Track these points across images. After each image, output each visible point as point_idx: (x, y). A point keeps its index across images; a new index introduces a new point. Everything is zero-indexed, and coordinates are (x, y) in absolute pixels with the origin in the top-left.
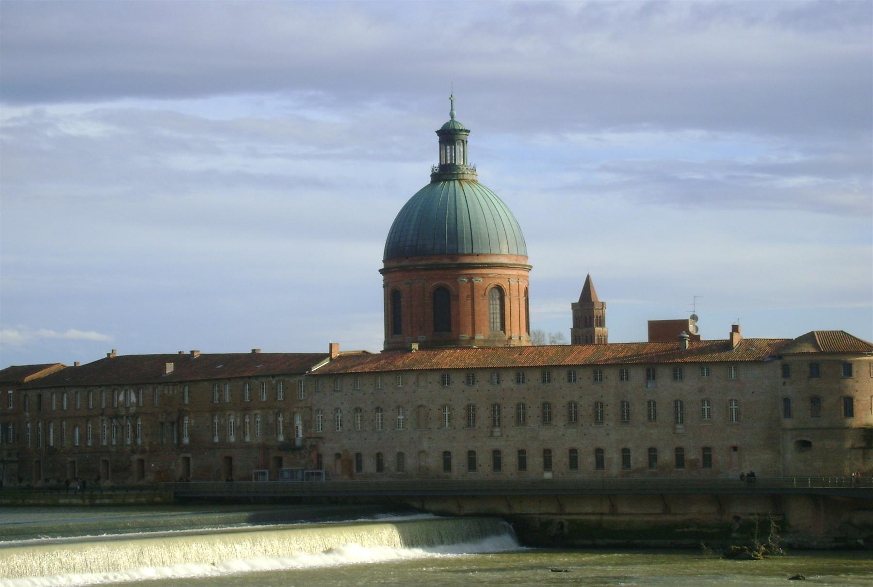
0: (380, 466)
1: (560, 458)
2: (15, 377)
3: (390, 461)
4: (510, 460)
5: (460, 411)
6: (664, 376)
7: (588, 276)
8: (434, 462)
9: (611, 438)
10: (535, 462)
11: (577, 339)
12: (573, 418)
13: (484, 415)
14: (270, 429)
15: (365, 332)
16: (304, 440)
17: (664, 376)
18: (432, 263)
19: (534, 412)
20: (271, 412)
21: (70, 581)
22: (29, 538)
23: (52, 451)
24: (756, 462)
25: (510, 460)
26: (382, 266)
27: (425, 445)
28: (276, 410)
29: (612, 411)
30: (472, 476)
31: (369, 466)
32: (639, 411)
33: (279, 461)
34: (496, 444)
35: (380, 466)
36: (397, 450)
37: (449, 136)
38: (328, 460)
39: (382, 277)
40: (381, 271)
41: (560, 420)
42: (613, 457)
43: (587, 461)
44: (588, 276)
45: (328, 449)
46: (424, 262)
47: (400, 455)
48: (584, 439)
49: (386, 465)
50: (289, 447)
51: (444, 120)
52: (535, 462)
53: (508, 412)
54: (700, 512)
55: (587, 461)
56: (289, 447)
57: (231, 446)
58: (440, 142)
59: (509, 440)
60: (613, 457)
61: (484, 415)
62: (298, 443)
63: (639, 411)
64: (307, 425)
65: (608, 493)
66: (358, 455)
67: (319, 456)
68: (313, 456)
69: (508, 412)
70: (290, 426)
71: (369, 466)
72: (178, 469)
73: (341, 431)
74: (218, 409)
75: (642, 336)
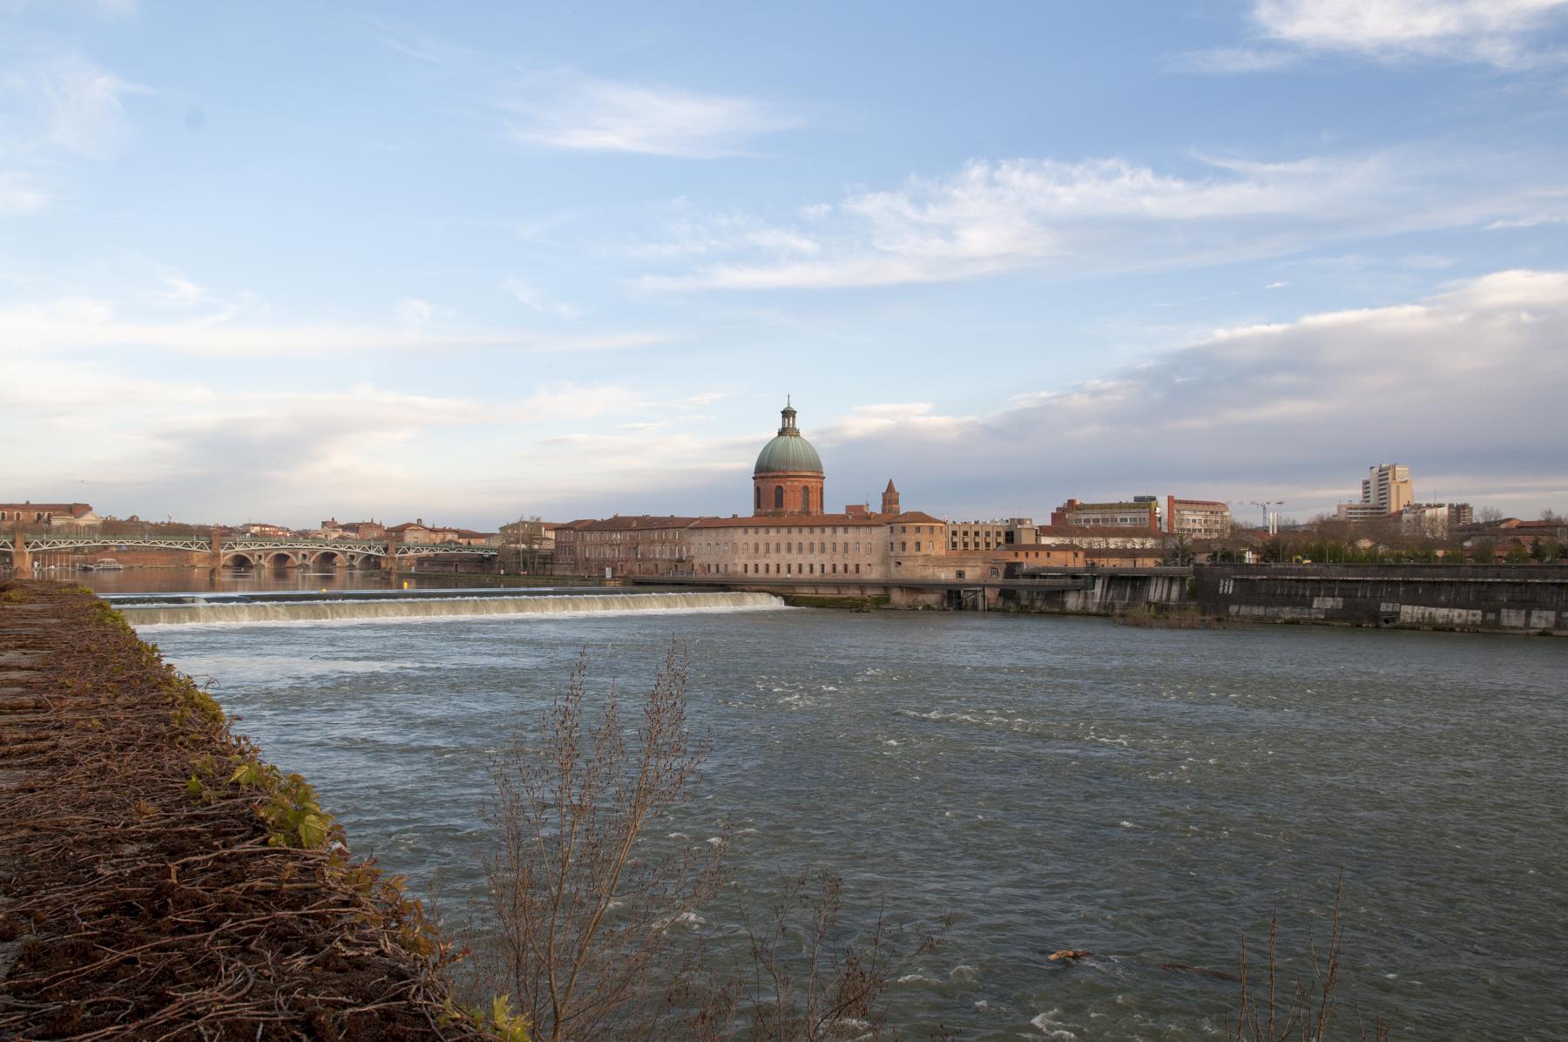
1: (794, 568)
3: (722, 568)
4: (773, 569)
5: (752, 546)
7: (890, 484)
8: (740, 569)
9: (817, 559)
10: (784, 569)
11: (884, 510)
12: (800, 550)
13: (762, 548)
14: (672, 552)
17: (840, 530)
19: (783, 547)
21: (960, 574)
23: (587, 560)
24: (875, 574)
29: (817, 547)
31: (713, 569)
32: (829, 547)
34: (789, 557)
37: (788, 414)
42: (817, 568)
43: (806, 569)
44: (890, 484)
45: (696, 562)
48: (805, 559)
50: (680, 560)
51: (783, 407)
52: (784, 569)
53: (772, 547)
54: (854, 593)
59: (773, 560)
60: (817, 568)
61: (762, 548)
63: (829, 547)
69: (772, 547)
71: (713, 569)
72: (636, 569)
73: (703, 552)
74: (652, 542)
75: (1132, 501)
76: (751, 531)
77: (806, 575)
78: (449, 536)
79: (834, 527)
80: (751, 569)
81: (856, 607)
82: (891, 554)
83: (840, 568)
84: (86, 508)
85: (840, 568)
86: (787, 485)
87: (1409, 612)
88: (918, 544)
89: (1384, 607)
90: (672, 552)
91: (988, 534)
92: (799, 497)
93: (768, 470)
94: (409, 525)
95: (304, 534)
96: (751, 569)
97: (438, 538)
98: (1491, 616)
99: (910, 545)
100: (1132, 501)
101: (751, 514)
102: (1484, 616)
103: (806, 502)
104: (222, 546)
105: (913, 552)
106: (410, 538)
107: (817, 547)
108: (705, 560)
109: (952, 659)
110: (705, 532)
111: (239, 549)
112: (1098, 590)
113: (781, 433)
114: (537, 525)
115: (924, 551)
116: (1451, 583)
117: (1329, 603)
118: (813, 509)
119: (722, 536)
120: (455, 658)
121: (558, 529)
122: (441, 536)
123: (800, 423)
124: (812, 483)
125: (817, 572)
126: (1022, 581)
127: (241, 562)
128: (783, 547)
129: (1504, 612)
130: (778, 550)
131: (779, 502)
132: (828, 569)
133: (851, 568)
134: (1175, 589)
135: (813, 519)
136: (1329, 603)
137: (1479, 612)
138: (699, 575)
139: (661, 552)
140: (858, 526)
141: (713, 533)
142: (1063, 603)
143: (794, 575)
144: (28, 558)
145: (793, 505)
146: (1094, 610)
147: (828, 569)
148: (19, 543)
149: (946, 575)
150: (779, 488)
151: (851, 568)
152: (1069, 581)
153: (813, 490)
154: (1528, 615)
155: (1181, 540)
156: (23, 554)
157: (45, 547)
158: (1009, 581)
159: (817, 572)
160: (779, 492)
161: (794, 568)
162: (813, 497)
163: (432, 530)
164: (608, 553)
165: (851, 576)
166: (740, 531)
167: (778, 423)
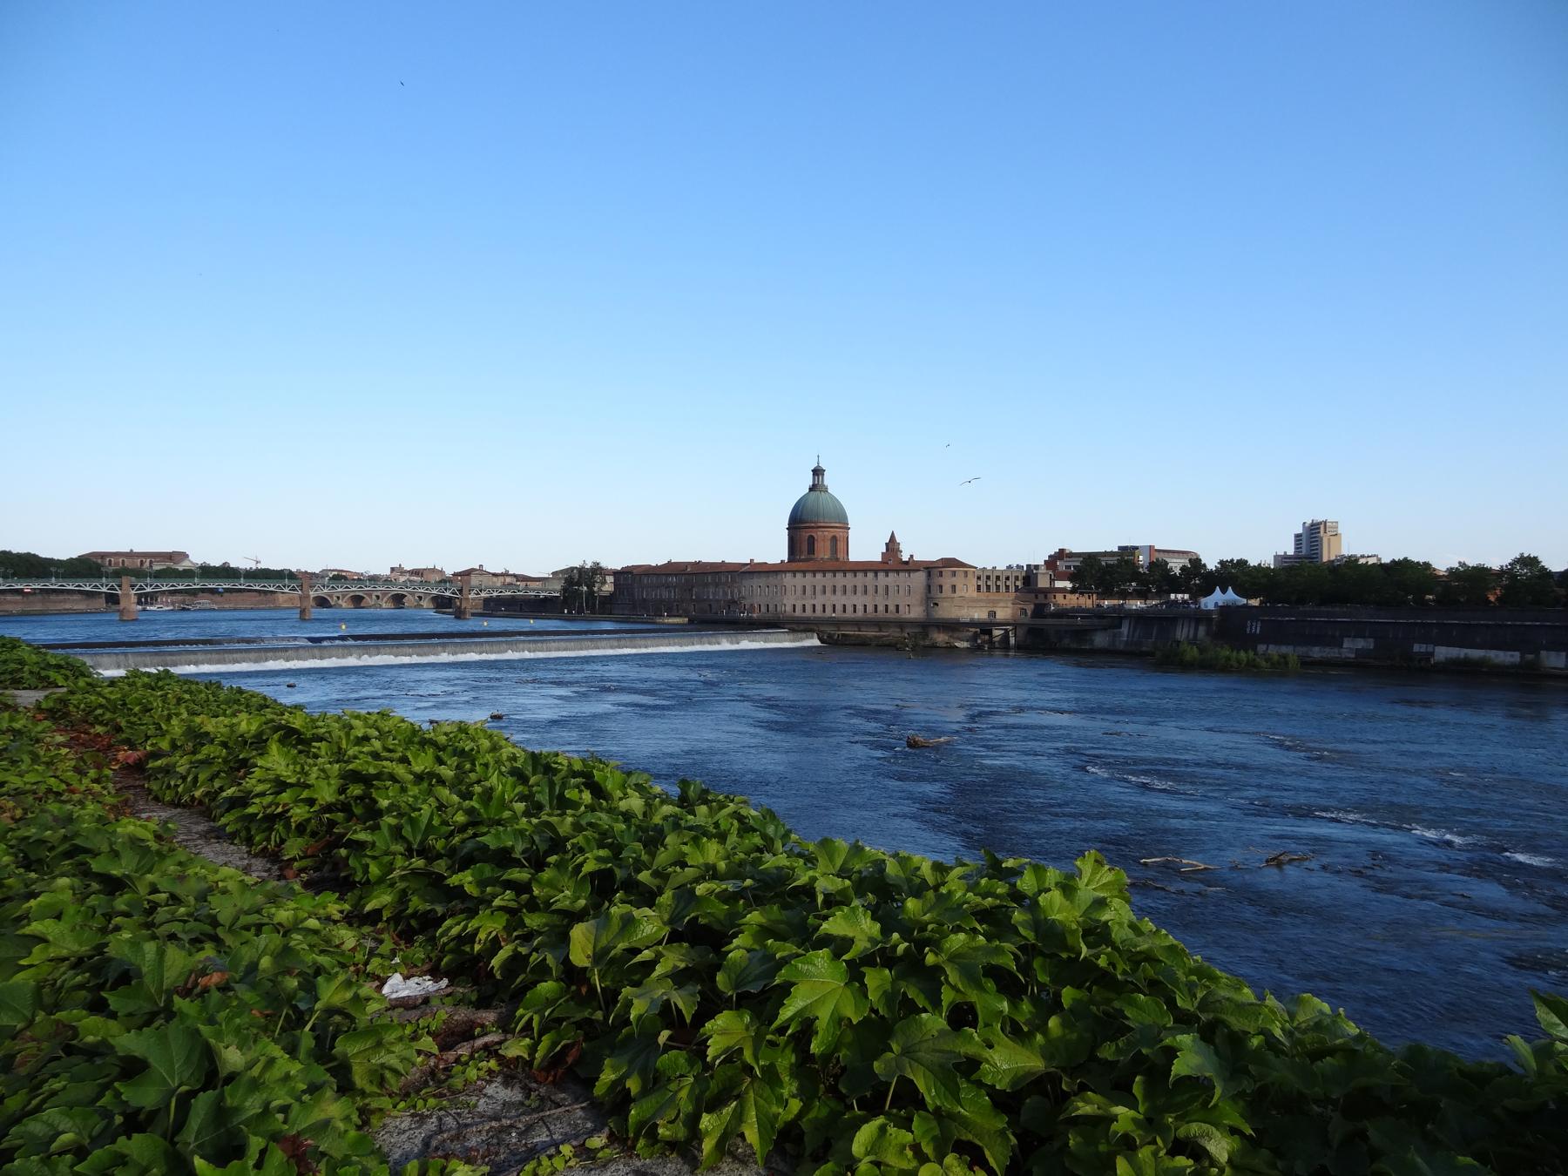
1: (839, 608)
2: (4, 553)
4: (819, 608)
5: (799, 589)
6: (881, 575)
7: (893, 536)
8: (789, 609)
9: (859, 600)
10: (829, 609)
15: (776, 550)
17: (881, 575)
18: (813, 528)
22: (305, 659)
25: (819, 608)
29: (860, 589)
30: (888, 615)
32: (871, 590)
34: (833, 598)
37: (818, 472)
41: (839, 593)
42: (860, 608)
43: (850, 609)
44: (893, 536)
51: (814, 465)
52: (829, 609)
53: (849, 588)
55: (850, 609)
59: (819, 601)
60: (860, 608)
63: (871, 590)
65: (857, 623)
73: (757, 596)
74: (707, 585)
77: (849, 614)
78: (508, 580)
79: (876, 572)
80: (799, 609)
81: (892, 646)
82: (930, 597)
83: (881, 608)
84: (184, 556)
85: (881, 608)
86: (818, 534)
87: (1442, 653)
88: (954, 587)
89: (1416, 648)
90: (725, 594)
91: (998, 578)
92: (828, 544)
93: (802, 521)
94: (473, 570)
95: (374, 579)
96: (799, 609)
97: (499, 582)
98: (1530, 657)
99: (947, 588)
103: (835, 550)
104: (312, 587)
105: (950, 594)
106: (474, 581)
107: (860, 589)
109: (414, 714)
111: (319, 593)
112: (1125, 630)
113: (813, 488)
114: (597, 570)
115: (958, 593)
116: (1487, 626)
117: (1361, 644)
118: (840, 556)
119: (772, 580)
120: (633, 672)
121: (616, 573)
122: (501, 579)
123: (828, 480)
124: (839, 533)
125: (860, 613)
126: (1050, 621)
127: (322, 602)
128: (828, 590)
129: (1543, 653)
130: (834, 592)
131: (811, 550)
132: (870, 609)
133: (892, 608)
134: (1202, 630)
136: (1361, 644)
137: (1517, 654)
140: (898, 571)
142: (1092, 641)
143: (839, 614)
144: (134, 599)
145: (823, 552)
146: (1122, 647)
147: (870, 609)
148: (125, 586)
149: (980, 614)
150: (834, 539)
151: (892, 608)
152: (1096, 621)
153: (839, 543)
155: (930, 597)
156: (128, 595)
157: (149, 590)
158: (1039, 621)
159: (819, 612)
160: (812, 540)
161: (839, 608)
162: (840, 545)
163: (495, 575)
164: (665, 595)
165: (891, 615)
166: (789, 575)
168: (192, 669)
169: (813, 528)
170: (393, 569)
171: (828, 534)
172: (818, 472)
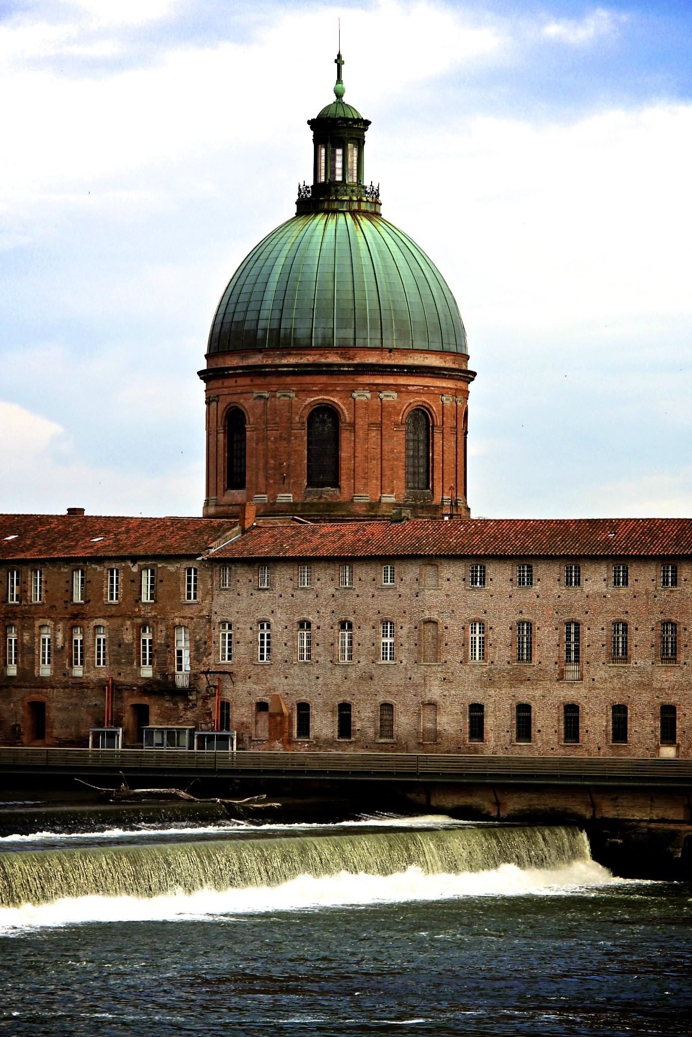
0: (345, 727)
3: (364, 719)
5: (502, 634)
8: (451, 723)
13: (548, 641)
14: (122, 654)
16: (194, 677)
20: (129, 623)
25: (596, 724)
26: (203, 365)
27: (435, 692)
28: (140, 621)
30: (523, 751)
31: (324, 725)
33: (142, 713)
35: (345, 727)
36: (381, 699)
37: (337, 130)
38: (241, 714)
39: (202, 385)
40: (199, 373)
45: (242, 697)
46: (292, 360)
47: (387, 707)
49: (357, 725)
50: (163, 687)
51: (320, 101)
53: (595, 636)
56: (163, 687)
57: (43, 683)
58: (317, 141)
61: (548, 641)
62: (182, 680)
64: (200, 650)
66: (304, 709)
67: (225, 707)
68: (213, 705)
69: (595, 636)
70: (163, 653)
71: (324, 725)
75: (65, 513)
76: (548, 577)
79: (85, 562)
86: (357, 400)
92: (397, 443)
100: (65, 513)
101: (198, 513)
102: (428, 800)
103: (422, 471)
108: (287, 685)
110: (283, 576)
113: (316, 201)
123: (380, 163)
124: (434, 393)
130: (619, 652)
131: (325, 467)
135: (440, 533)
138: (253, 745)
139: (62, 656)
141: (324, 581)
145: (375, 475)
150: (422, 418)
154: (594, 816)
160: (325, 426)
166: (454, 574)
167: (299, 166)
168: (66, 809)
169: (321, 385)
170: (69, 510)
171: (398, 398)
172: (337, 130)
